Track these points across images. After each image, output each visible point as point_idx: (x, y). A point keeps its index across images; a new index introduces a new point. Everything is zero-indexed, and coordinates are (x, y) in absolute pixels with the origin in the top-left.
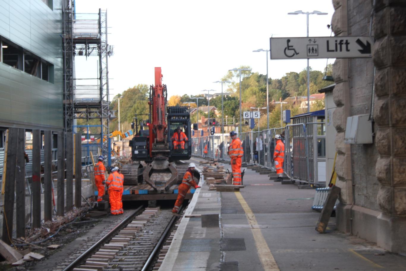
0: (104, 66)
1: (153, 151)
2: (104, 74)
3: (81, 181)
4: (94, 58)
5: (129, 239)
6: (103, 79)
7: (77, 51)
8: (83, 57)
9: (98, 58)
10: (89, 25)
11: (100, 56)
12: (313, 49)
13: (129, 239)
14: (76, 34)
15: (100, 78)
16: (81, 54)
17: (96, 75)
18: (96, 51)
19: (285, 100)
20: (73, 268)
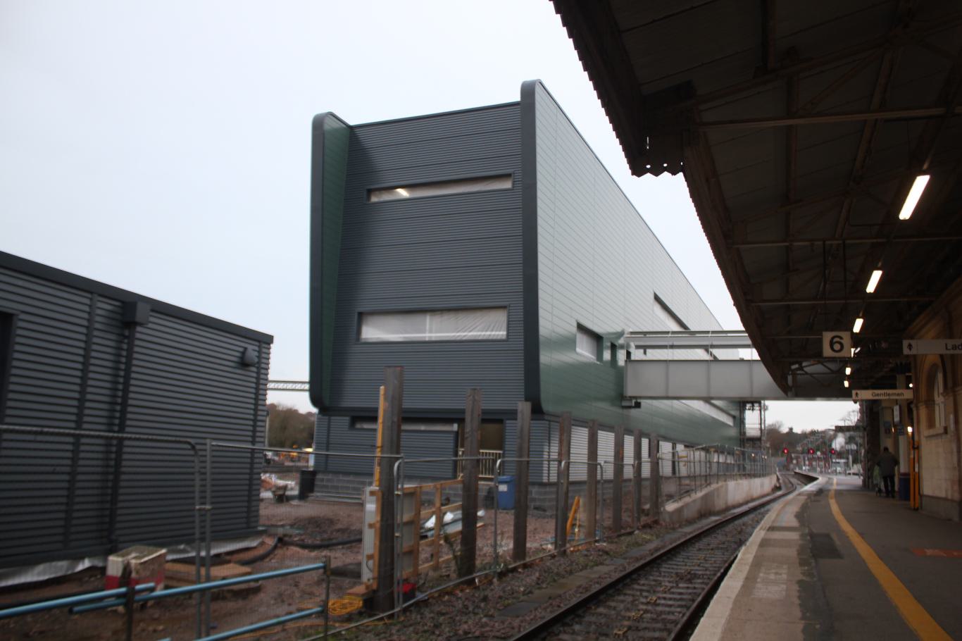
0: (763, 417)
1: (576, 498)
2: (763, 422)
3: (478, 484)
4: (757, 412)
5: (681, 585)
6: (452, 447)
7: (747, 408)
8: (751, 412)
9: (759, 412)
10: (675, 402)
11: (760, 410)
12: (202, 486)
13: (681, 585)
14: (746, 400)
15: (761, 424)
16: (749, 409)
17: (758, 421)
18: (758, 408)
19: (395, 606)
20: (437, 518)
